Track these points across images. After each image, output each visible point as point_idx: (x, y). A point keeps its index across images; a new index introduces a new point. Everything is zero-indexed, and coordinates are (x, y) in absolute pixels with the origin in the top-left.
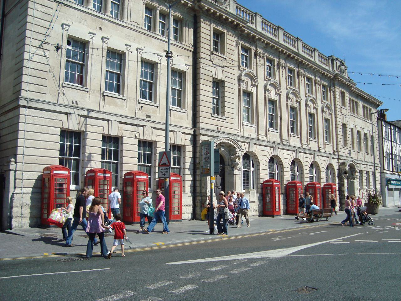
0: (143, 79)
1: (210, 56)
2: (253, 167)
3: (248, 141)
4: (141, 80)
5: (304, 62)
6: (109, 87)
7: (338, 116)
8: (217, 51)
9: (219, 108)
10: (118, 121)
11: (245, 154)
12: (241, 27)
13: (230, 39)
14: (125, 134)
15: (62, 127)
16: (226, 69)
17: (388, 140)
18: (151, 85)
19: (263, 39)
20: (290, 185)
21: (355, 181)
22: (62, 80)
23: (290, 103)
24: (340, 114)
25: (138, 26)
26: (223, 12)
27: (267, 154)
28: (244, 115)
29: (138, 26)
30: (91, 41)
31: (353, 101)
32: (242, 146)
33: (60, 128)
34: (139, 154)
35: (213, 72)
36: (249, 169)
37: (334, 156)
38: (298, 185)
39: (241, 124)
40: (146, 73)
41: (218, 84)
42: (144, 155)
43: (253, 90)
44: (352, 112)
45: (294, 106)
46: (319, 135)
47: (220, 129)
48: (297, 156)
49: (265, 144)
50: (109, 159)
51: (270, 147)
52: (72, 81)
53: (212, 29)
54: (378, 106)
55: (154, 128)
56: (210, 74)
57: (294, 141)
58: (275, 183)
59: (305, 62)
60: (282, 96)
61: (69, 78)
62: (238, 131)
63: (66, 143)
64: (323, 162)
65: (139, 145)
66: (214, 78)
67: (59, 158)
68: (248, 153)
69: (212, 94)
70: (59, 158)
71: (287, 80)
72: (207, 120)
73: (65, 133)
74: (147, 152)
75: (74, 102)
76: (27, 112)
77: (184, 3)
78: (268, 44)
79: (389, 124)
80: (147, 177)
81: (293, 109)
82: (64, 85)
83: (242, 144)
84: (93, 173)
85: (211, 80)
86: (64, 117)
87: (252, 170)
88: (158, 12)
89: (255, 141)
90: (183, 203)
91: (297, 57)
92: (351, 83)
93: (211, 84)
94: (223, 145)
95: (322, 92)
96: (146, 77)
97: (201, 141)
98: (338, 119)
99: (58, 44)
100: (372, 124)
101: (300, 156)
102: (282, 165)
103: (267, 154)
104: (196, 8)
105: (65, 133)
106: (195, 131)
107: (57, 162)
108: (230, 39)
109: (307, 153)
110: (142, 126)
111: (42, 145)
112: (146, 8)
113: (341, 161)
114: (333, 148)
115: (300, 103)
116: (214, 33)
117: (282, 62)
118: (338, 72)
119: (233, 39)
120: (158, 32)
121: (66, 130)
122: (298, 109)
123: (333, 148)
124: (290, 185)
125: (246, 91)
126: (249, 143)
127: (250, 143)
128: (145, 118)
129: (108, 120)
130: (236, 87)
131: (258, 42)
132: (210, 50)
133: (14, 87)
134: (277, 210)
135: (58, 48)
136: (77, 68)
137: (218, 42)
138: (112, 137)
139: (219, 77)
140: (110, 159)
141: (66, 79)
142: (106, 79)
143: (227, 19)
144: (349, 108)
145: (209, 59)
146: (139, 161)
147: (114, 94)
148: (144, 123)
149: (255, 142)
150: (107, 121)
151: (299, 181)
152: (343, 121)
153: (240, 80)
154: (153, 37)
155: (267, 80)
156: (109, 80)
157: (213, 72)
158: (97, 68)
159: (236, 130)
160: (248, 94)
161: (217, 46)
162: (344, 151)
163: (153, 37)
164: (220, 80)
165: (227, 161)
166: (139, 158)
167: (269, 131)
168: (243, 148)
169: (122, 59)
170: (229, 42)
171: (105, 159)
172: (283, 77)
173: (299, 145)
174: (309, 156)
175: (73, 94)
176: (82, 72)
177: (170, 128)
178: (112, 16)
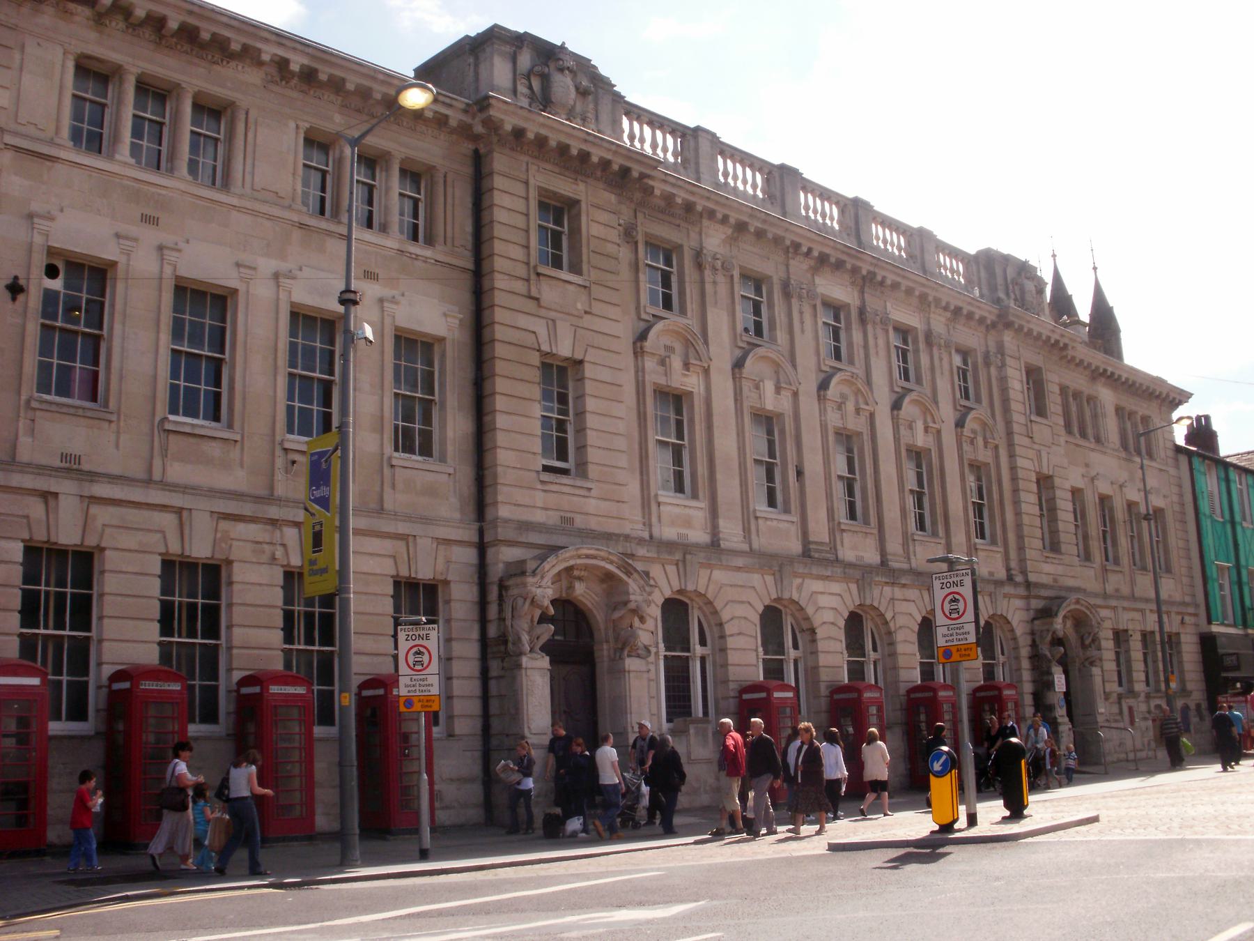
0: (299, 371)
1: (528, 280)
2: (703, 642)
4: (396, 395)
5: (879, 278)
6: (184, 402)
7: (1018, 450)
8: (557, 263)
9: (563, 448)
15: (163, 550)
16: (587, 321)
20: (983, 694)
22: (29, 388)
23: (833, 419)
24: (1026, 441)
28: (661, 464)
36: (688, 650)
38: (942, 694)
39: (647, 501)
40: (309, 352)
43: (692, 383)
46: (952, 523)
47: (571, 521)
48: (868, 595)
50: (306, 643)
52: (64, 390)
53: (533, 194)
55: (95, 500)
56: (530, 340)
58: (776, 695)
59: (884, 278)
60: (802, 398)
61: (55, 381)
63: (43, 588)
65: (396, 597)
72: (524, 496)
74: (69, 590)
75: (64, 457)
80: (311, 691)
81: (847, 439)
82: (34, 404)
84: (255, 685)
85: (535, 359)
86: (169, 520)
93: (535, 375)
94: (583, 573)
95: (893, 352)
96: (196, 340)
97: (501, 566)
98: (1021, 462)
99: (16, 278)
101: (881, 595)
102: (813, 631)
104: (479, 129)
106: (481, 533)
108: (600, 220)
116: (543, 206)
121: (46, 546)
122: (865, 437)
124: (983, 694)
125: (667, 390)
126: (680, 564)
129: (179, 511)
130: (627, 381)
131: (705, 222)
132: (528, 264)
136: (316, 392)
139: (564, 349)
140: (310, 641)
141: (44, 387)
142: (290, 397)
145: (524, 291)
147: (201, 424)
150: (402, 539)
151: (1008, 681)
158: (140, 346)
160: (676, 400)
161: (557, 244)
162: (1047, 568)
164: (567, 359)
165: (602, 626)
167: (757, 518)
170: (596, 230)
173: (873, 557)
175: (63, 432)
176: (218, 383)
177: (1164, 608)
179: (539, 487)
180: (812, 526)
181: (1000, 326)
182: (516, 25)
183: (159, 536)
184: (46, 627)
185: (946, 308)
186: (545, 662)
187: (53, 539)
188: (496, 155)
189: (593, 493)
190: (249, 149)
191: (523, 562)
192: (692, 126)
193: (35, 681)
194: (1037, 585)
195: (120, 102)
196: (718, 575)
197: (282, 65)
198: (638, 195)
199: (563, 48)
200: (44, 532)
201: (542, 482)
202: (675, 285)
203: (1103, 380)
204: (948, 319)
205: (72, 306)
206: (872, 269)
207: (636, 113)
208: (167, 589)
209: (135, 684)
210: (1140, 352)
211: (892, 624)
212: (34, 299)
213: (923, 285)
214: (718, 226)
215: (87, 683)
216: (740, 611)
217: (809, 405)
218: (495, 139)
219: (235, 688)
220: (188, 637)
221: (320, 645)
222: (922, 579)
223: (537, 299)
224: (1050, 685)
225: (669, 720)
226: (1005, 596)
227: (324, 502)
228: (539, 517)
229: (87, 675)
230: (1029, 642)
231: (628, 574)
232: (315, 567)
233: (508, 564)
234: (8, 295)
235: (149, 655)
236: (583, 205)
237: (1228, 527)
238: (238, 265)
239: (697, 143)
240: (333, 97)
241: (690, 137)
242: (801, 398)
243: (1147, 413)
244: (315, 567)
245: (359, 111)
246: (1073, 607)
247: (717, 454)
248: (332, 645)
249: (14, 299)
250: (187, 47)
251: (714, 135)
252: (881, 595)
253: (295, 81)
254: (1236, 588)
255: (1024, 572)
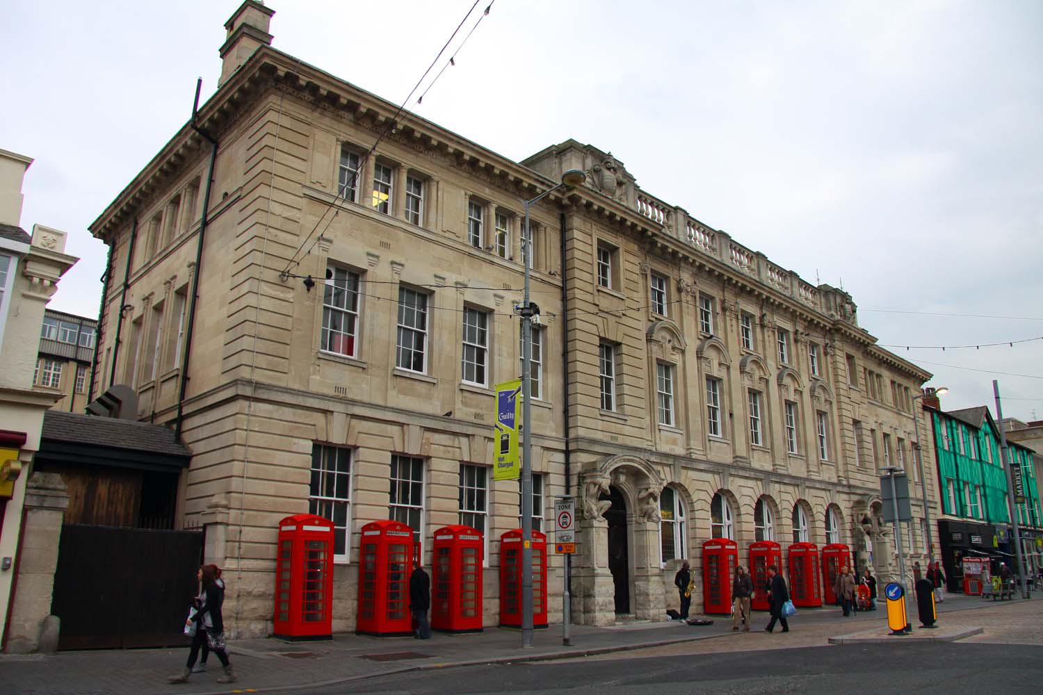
3: (671, 462)
5: (772, 301)
10: (421, 427)
11: (665, 488)
12: (650, 237)
13: (630, 261)
14: (434, 451)
17: (961, 456)
18: (481, 353)
19: (692, 258)
21: (886, 539)
24: (847, 400)
25: (456, 239)
26: (616, 208)
27: (706, 486)
29: (456, 239)
30: (370, 269)
31: (871, 373)
32: (659, 472)
33: (313, 440)
34: (393, 484)
35: (601, 326)
37: (840, 489)
39: (653, 428)
41: (609, 347)
42: (330, 477)
43: (676, 358)
44: (870, 396)
45: (756, 388)
49: (702, 466)
51: (757, 479)
54: (923, 381)
55: (354, 416)
56: (594, 329)
57: (759, 460)
62: (650, 443)
64: (819, 501)
65: (393, 466)
66: (601, 339)
67: (309, 500)
68: (670, 487)
69: (598, 369)
70: (309, 500)
71: (651, 301)
72: (589, 424)
73: (322, 449)
74: (336, 472)
76: (252, 409)
77: (420, 138)
78: (701, 267)
79: (947, 417)
81: (754, 393)
83: (659, 468)
85: (597, 341)
86: (395, 430)
87: (679, 521)
88: (493, 212)
89: (683, 462)
90: (549, 590)
91: (757, 290)
92: (867, 338)
93: (597, 351)
100: (914, 419)
103: (706, 486)
104: (566, 201)
105: (322, 449)
107: (305, 509)
109: (785, 484)
110: (467, 436)
111: (278, 473)
112: (344, 153)
113: (855, 498)
114: (838, 470)
115: (767, 381)
117: (729, 297)
118: (839, 317)
119: (636, 260)
120: (402, 217)
123: (838, 470)
127: (674, 465)
128: (472, 419)
129: (402, 425)
130: (643, 354)
133: (225, 359)
134: (816, 596)
135: (309, 283)
137: (607, 267)
138: (409, 458)
143: (623, 221)
144: (864, 388)
146: (393, 500)
148: (470, 430)
149: (683, 463)
152: (855, 414)
153: (649, 340)
154: (484, 260)
155: (654, 319)
156: (477, 362)
157: (601, 326)
158: (379, 320)
159: (648, 440)
160: (666, 366)
162: (859, 476)
163: (484, 260)
166: (392, 493)
168: (662, 476)
169: (428, 305)
171: (318, 495)
172: (732, 331)
173: (769, 468)
174: (790, 489)
178: (406, 221)
179: (600, 418)
180: (737, 447)
181: (833, 331)
182: (584, 140)
183: (391, 439)
184: (322, 495)
185: (805, 320)
186: (605, 524)
187: (330, 441)
188: (575, 218)
189: (628, 423)
190: (440, 206)
191: (594, 463)
192: (674, 205)
193: (327, 529)
194: (854, 487)
195: (367, 173)
196: (691, 474)
197: (458, 155)
198: (647, 247)
199: (609, 155)
200: (324, 435)
201: (601, 415)
202: (664, 301)
203: (885, 365)
204: (805, 327)
205: (339, 294)
206: (768, 295)
207: (643, 197)
208: (316, 464)
209: (456, 537)
210: (102, 241)
211: (779, 507)
212: (320, 290)
213: (795, 306)
214: (689, 267)
215: (345, 530)
216: (703, 495)
217: (735, 373)
218: (575, 208)
219: (360, 531)
220: (403, 503)
221: (337, 497)
222: (828, 486)
223: (598, 305)
224: (863, 547)
225: (664, 561)
226: (838, 492)
227: (510, 423)
228: (599, 436)
229: (345, 526)
230: (850, 520)
231: (649, 471)
232: (503, 462)
233: (584, 465)
234: (305, 287)
235: (383, 515)
236: (621, 250)
237: (952, 455)
238: (436, 276)
239: (677, 217)
240: (485, 178)
241: (669, 210)
242: (731, 370)
243: (908, 386)
244: (503, 462)
245: (499, 187)
246: (875, 500)
247: (689, 402)
248: (346, 497)
249: (308, 290)
250: (405, 141)
251: (685, 212)
252: (774, 490)
253: (465, 166)
254: (957, 493)
255: (847, 478)
